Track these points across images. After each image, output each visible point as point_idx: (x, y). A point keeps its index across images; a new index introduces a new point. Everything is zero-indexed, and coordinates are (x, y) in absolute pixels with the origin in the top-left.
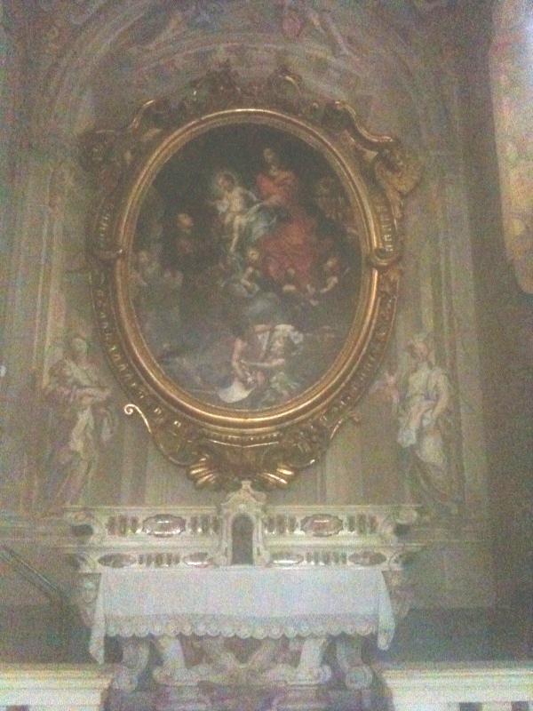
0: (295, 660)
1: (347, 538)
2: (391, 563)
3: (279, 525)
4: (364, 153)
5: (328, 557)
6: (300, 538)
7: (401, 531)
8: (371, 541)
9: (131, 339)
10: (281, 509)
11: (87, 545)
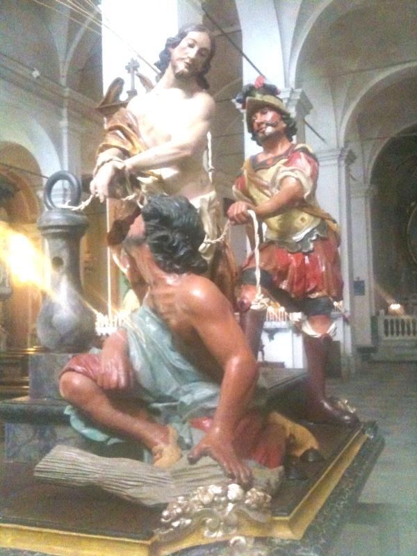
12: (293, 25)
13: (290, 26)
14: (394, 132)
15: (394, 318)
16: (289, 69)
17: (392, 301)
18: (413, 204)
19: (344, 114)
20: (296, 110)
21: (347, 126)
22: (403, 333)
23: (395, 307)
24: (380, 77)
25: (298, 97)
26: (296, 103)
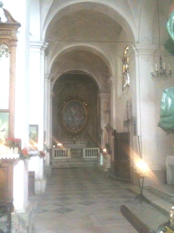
0: (79, 151)
1: (83, 142)
2: (87, 144)
3: (78, 141)
4: (67, 142)
5: (81, 143)
6: (79, 142)
7: (88, 141)
8: (85, 142)
9: (63, 109)
10: (78, 139)
11: (131, 118)
12: (47, 13)
13: (45, 13)
14: (65, 71)
15: (59, 149)
16: (42, 33)
17: (59, 142)
18: (65, 102)
19: (50, 61)
20: (45, 52)
21: (52, 66)
22: (62, 156)
23: (60, 144)
24: (67, 47)
25: (46, 47)
26: (45, 49)
